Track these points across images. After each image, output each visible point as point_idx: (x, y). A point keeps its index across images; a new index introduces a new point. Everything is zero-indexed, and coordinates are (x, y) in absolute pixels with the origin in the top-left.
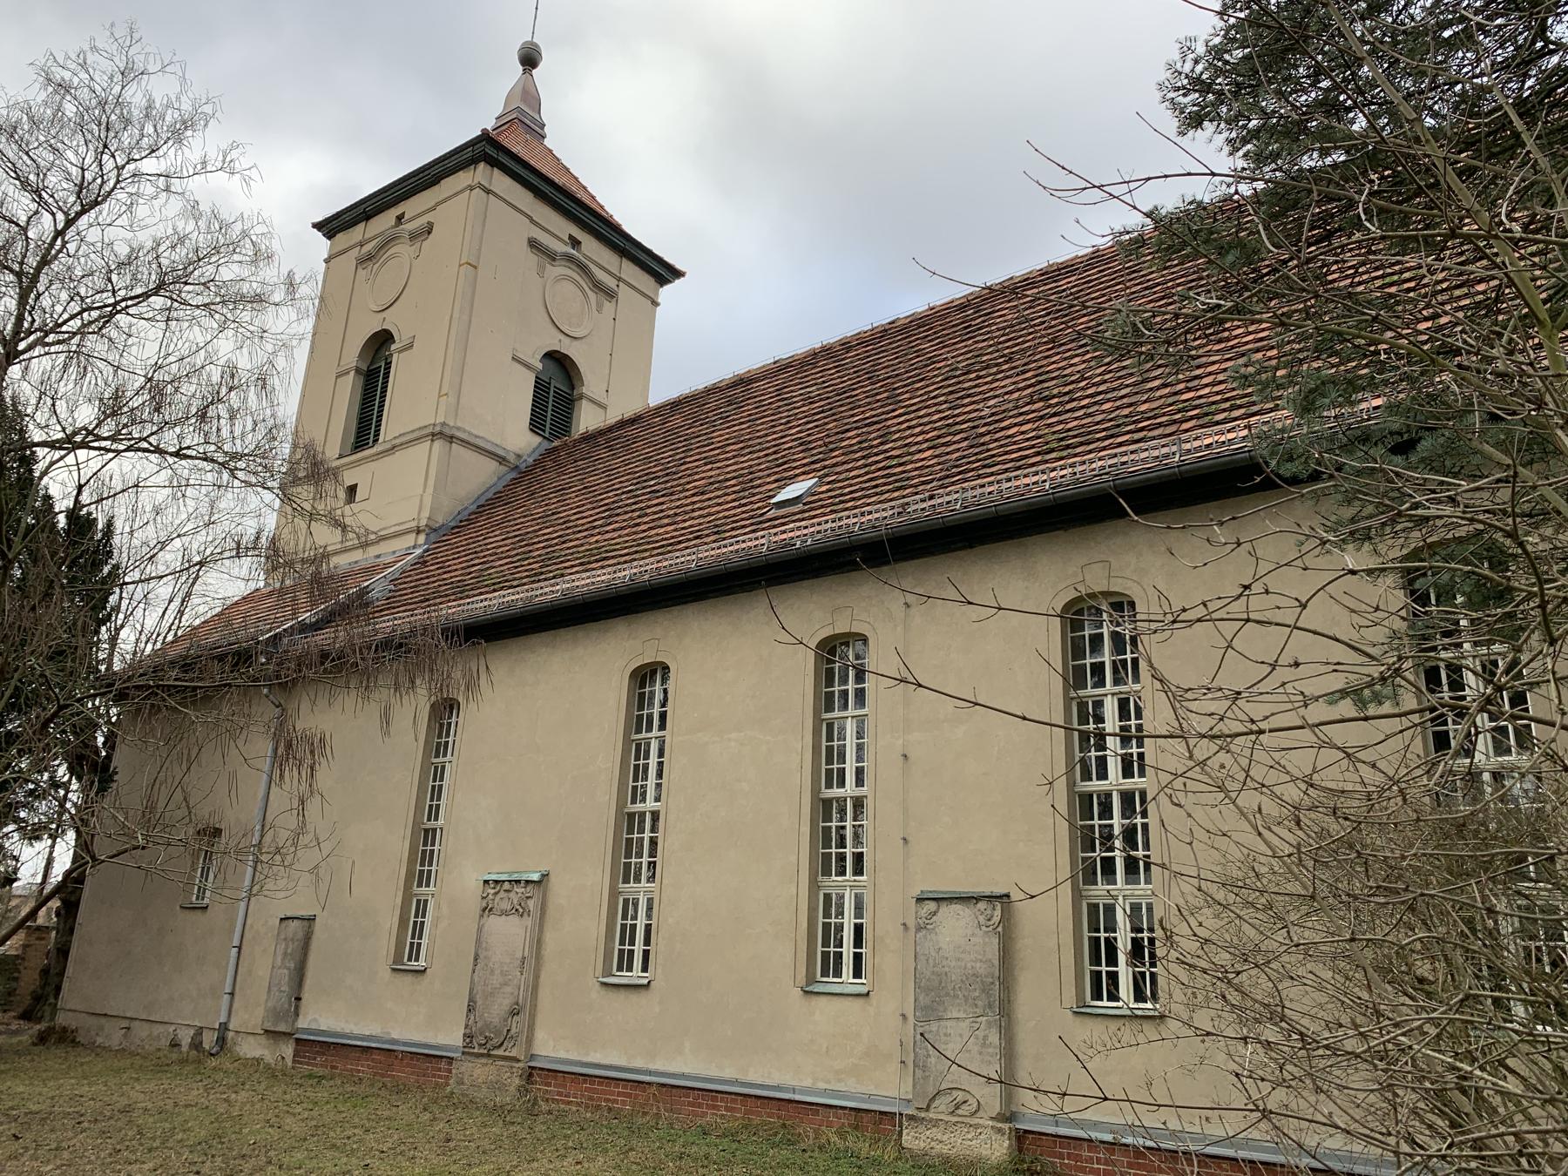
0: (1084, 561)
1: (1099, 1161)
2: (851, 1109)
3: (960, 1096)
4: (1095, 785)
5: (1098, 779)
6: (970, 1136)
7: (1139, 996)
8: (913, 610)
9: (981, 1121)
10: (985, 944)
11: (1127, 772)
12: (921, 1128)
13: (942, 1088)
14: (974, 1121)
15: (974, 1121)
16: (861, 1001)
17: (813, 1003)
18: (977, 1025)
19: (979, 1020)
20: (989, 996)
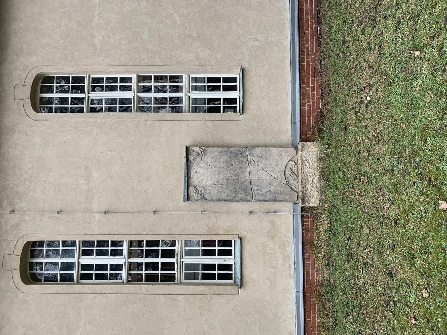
0: (12, 98)
1: (309, 102)
2: (303, 247)
3: (288, 172)
4: (133, 105)
5: (131, 104)
6: (308, 164)
7: (233, 88)
8: (17, 208)
9: (299, 158)
10: (211, 156)
11: (129, 89)
12: (308, 194)
13: (286, 183)
14: (300, 163)
15: (300, 163)
16: (244, 243)
17: (247, 280)
18: (252, 161)
19: (249, 160)
20: (237, 154)
